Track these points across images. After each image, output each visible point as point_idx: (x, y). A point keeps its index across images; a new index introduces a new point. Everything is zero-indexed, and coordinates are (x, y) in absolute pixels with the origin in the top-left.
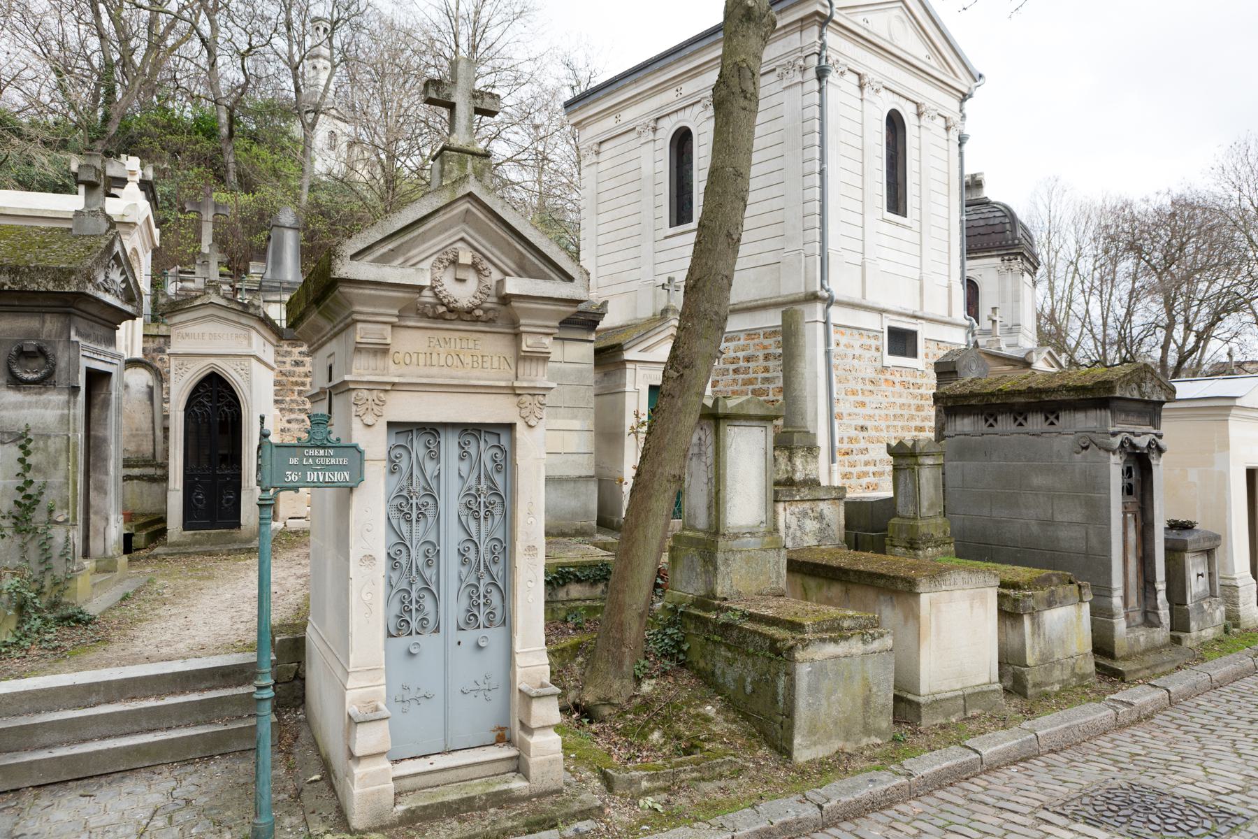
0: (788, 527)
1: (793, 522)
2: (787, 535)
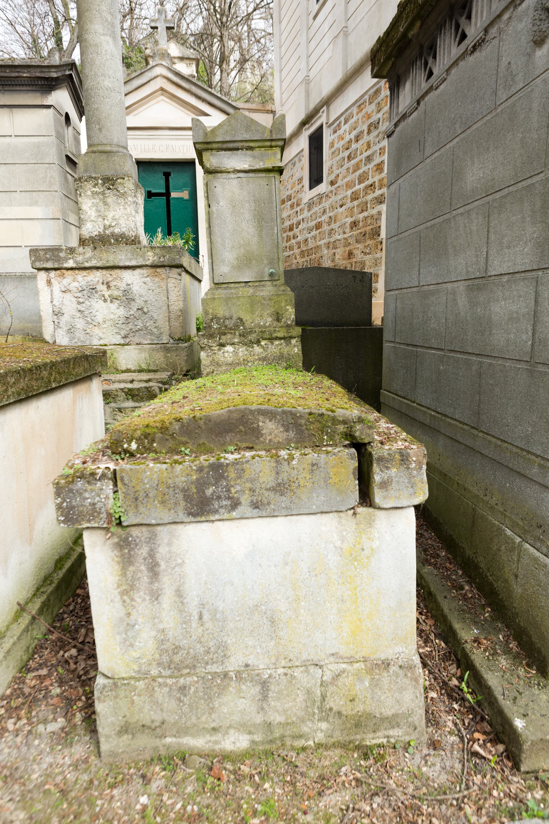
0: (58, 314)
1: (69, 305)
2: (57, 325)
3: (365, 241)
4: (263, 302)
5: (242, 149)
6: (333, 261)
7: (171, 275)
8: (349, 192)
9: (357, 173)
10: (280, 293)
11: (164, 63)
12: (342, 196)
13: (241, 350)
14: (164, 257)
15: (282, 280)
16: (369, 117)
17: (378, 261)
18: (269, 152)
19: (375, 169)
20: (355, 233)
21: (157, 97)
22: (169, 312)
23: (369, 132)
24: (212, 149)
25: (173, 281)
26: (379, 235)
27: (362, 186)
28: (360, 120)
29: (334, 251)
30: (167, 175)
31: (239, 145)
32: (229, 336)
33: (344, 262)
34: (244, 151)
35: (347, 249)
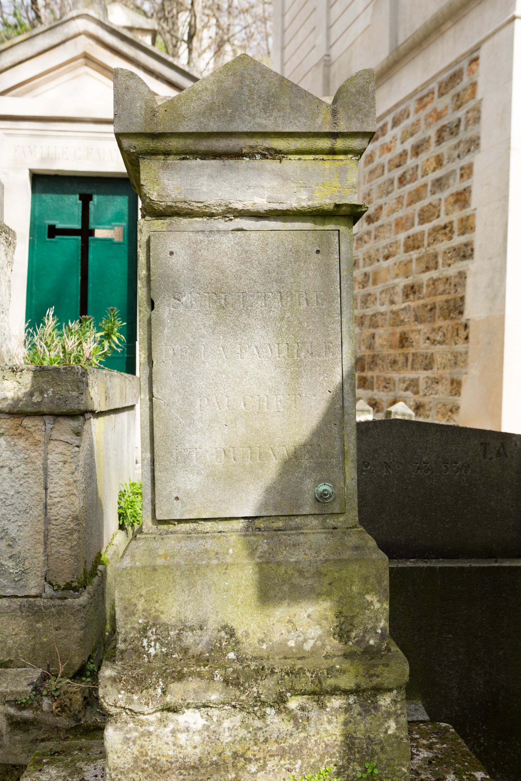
3: (433, 320)
4: (297, 580)
5: (251, 156)
6: (370, 347)
7: (55, 435)
8: (402, 236)
9: (418, 206)
10: (347, 554)
11: (92, 13)
12: (386, 242)
13: (226, 724)
14: (42, 393)
15: (352, 515)
16: (439, 116)
17: (460, 358)
18: (327, 165)
19: (452, 200)
20: (412, 304)
21: (76, 68)
22: (47, 521)
23: (440, 140)
24: (167, 153)
25: (61, 448)
26: (461, 313)
27: (427, 227)
28: (422, 122)
29: (372, 330)
30: (86, 199)
31: (245, 144)
32: (193, 684)
33: (392, 351)
34: (258, 162)
35: (399, 330)
